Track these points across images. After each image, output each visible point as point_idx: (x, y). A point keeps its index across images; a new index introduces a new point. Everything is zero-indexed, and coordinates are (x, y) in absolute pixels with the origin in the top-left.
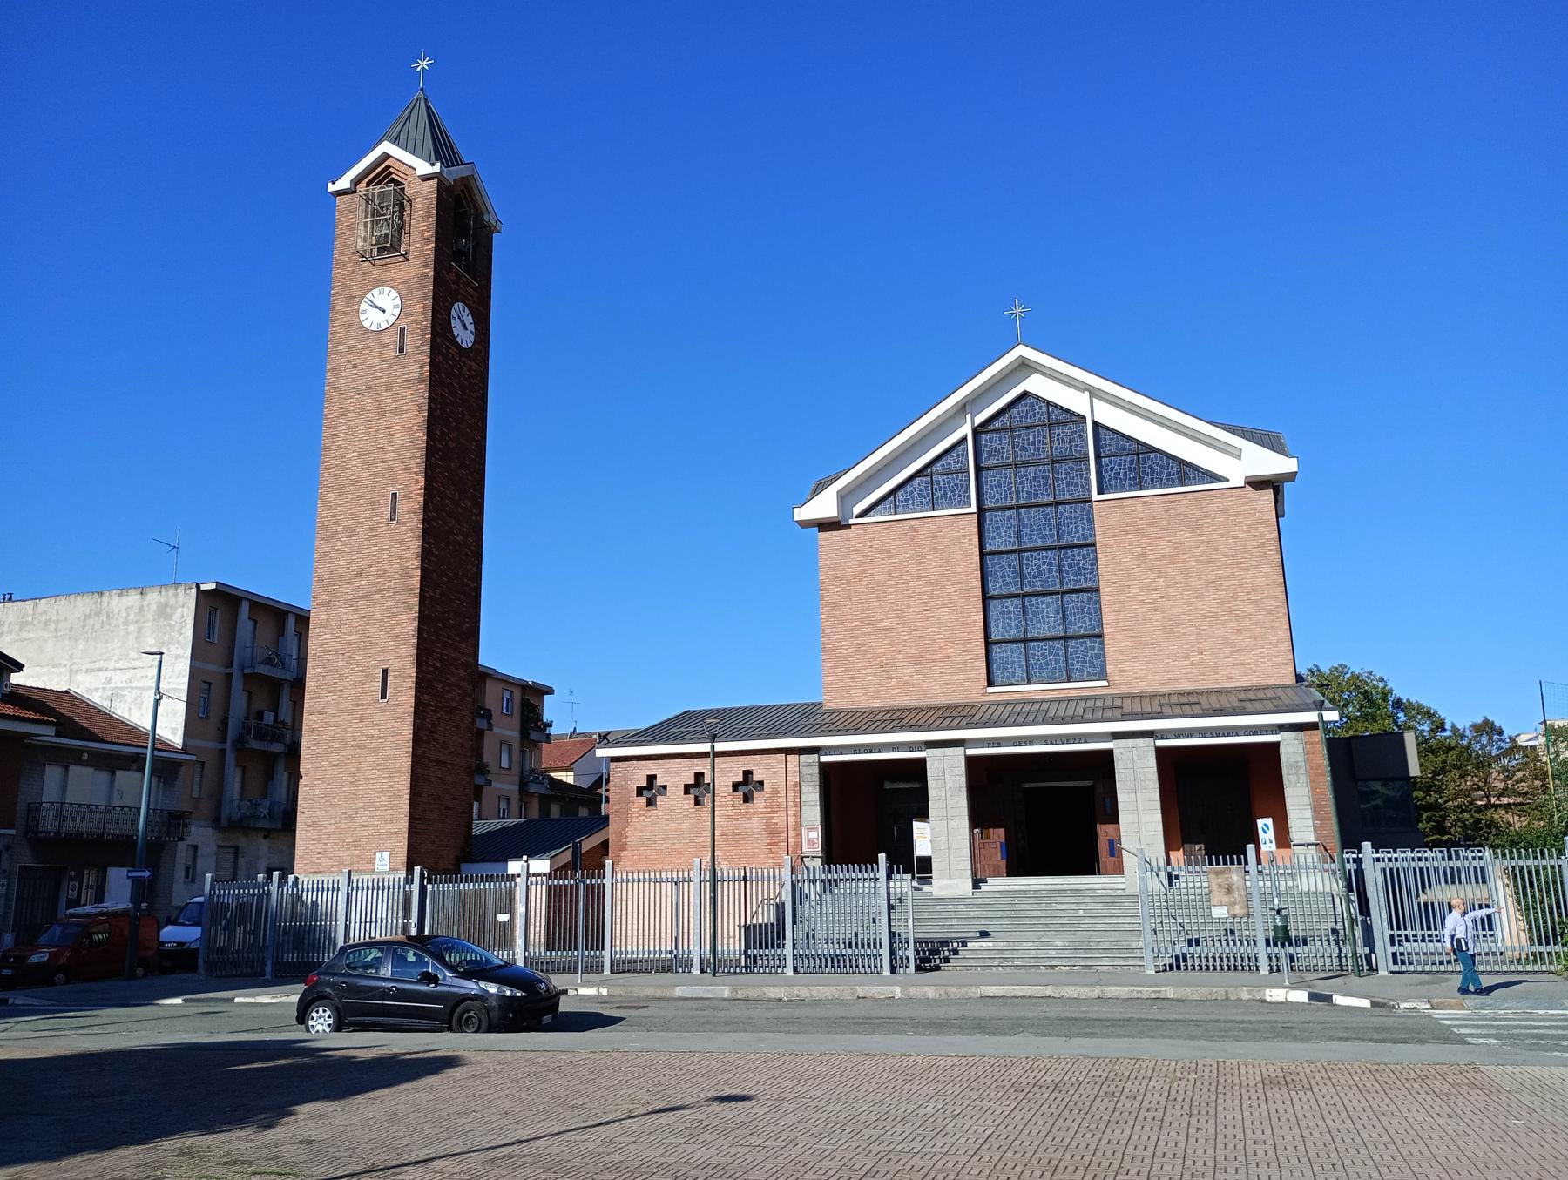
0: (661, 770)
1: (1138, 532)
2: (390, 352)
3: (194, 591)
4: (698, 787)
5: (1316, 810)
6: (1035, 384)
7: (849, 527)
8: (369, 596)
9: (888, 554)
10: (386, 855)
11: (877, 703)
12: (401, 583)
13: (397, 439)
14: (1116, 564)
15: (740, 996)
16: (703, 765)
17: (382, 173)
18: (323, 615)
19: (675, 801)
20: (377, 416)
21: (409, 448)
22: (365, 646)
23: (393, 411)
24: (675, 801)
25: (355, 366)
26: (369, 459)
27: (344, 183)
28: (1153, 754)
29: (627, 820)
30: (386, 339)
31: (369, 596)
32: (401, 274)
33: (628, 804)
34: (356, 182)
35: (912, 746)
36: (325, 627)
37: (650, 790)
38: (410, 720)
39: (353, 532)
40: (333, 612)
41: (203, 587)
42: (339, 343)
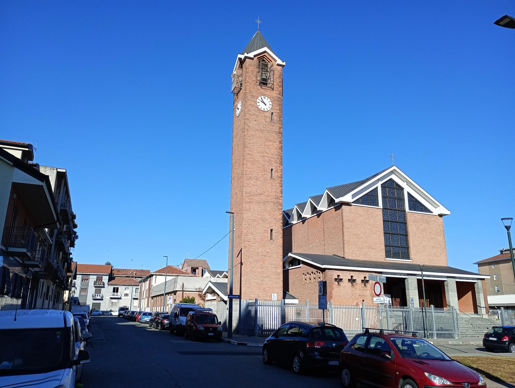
0: (356, 276)
1: (417, 222)
2: (268, 120)
3: (55, 171)
4: (352, 281)
5: (480, 299)
6: (394, 177)
7: (351, 205)
8: (264, 203)
9: (361, 216)
10: (276, 295)
11: (359, 259)
12: (276, 201)
13: (272, 150)
14: (411, 228)
15: (464, 344)
16: (367, 275)
17: (262, 59)
18: (248, 206)
19: (345, 283)
20: (265, 141)
21: (276, 155)
22: (264, 220)
23: (270, 141)
24: (345, 283)
25: (255, 121)
26: (262, 155)
27: (251, 55)
28: (455, 283)
29: (332, 289)
30: (266, 114)
31: (264, 203)
32: (271, 94)
33: (332, 283)
34: (255, 56)
35: (404, 274)
36: (249, 210)
37: (339, 280)
38: (281, 248)
39: (257, 179)
40: (252, 206)
41: (59, 170)
42: (249, 110)
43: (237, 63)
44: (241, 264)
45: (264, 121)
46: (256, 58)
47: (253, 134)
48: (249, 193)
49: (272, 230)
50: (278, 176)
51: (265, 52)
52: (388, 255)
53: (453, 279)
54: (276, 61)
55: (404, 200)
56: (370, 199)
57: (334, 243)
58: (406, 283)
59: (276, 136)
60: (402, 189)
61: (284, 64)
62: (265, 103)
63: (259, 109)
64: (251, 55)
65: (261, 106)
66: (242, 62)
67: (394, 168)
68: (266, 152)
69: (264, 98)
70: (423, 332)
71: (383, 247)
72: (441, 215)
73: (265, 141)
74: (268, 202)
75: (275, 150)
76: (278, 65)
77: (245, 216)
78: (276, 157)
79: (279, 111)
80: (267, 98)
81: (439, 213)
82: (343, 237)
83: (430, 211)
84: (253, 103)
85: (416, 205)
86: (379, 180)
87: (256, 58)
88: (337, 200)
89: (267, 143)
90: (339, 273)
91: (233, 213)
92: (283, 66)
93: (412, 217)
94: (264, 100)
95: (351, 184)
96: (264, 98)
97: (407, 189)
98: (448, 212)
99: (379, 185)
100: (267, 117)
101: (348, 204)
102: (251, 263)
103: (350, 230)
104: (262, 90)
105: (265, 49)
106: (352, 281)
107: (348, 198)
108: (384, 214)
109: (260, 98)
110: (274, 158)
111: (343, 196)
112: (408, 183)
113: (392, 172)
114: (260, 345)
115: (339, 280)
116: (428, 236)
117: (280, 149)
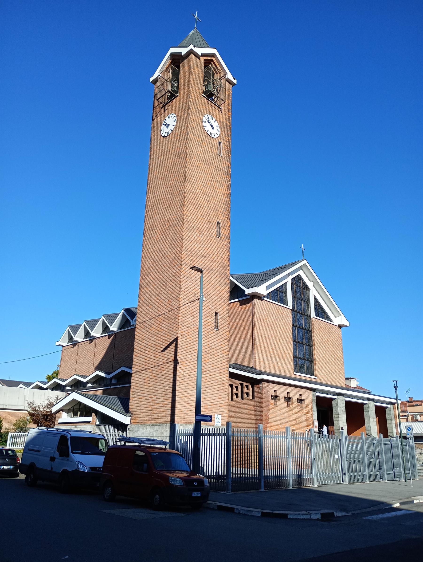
2: (215, 150)
4: (288, 399)
6: (301, 273)
7: (263, 300)
10: (220, 416)
12: (222, 270)
19: (281, 402)
23: (217, 181)
24: (281, 402)
25: (200, 146)
27: (199, 51)
29: (268, 410)
34: (204, 55)
36: (189, 278)
39: (201, 232)
43: (166, 60)
44: (176, 362)
45: (210, 151)
46: (202, 59)
47: (197, 164)
48: (191, 251)
49: (216, 313)
50: (225, 235)
51: (213, 55)
52: (295, 370)
53: (372, 402)
54: (226, 74)
55: (309, 303)
56: (278, 295)
57: (236, 347)
58: (333, 405)
59: (224, 178)
60: (308, 289)
61: (235, 81)
62: (213, 125)
63: (206, 132)
64: (199, 51)
65: (208, 128)
66: (177, 60)
67: (305, 262)
68: (212, 196)
69: (212, 118)
70: (395, 472)
71: (292, 358)
72: (340, 326)
73: (211, 179)
74: (213, 270)
75: (223, 197)
76: (228, 81)
77: (184, 285)
78: (224, 206)
79: (227, 144)
80: (214, 120)
81: (340, 323)
82: (253, 339)
83: (330, 319)
84: (197, 119)
85: (320, 311)
86: (289, 275)
87: (202, 59)
88: (248, 291)
89: (213, 183)
90: (275, 387)
91: (201, 271)
92: (233, 84)
93: (317, 324)
94: (212, 122)
95: (261, 274)
96: (212, 118)
97: (313, 292)
98: (347, 324)
99: (289, 280)
100: (214, 146)
101: (259, 297)
102: (190, 362)
103: (261, 331)
104: (208, 105)
105: (213, 51)
106: (288, 399)
107: (262, 290)
108: (293, 317)
109: (206, 116)
110: (221, 208)
111: (258, 286)
112: (315, 283)
113: (301, 268)
114: (314, 517)
115: (275, 397)
116: (330, 349)
117: (227, 197)
